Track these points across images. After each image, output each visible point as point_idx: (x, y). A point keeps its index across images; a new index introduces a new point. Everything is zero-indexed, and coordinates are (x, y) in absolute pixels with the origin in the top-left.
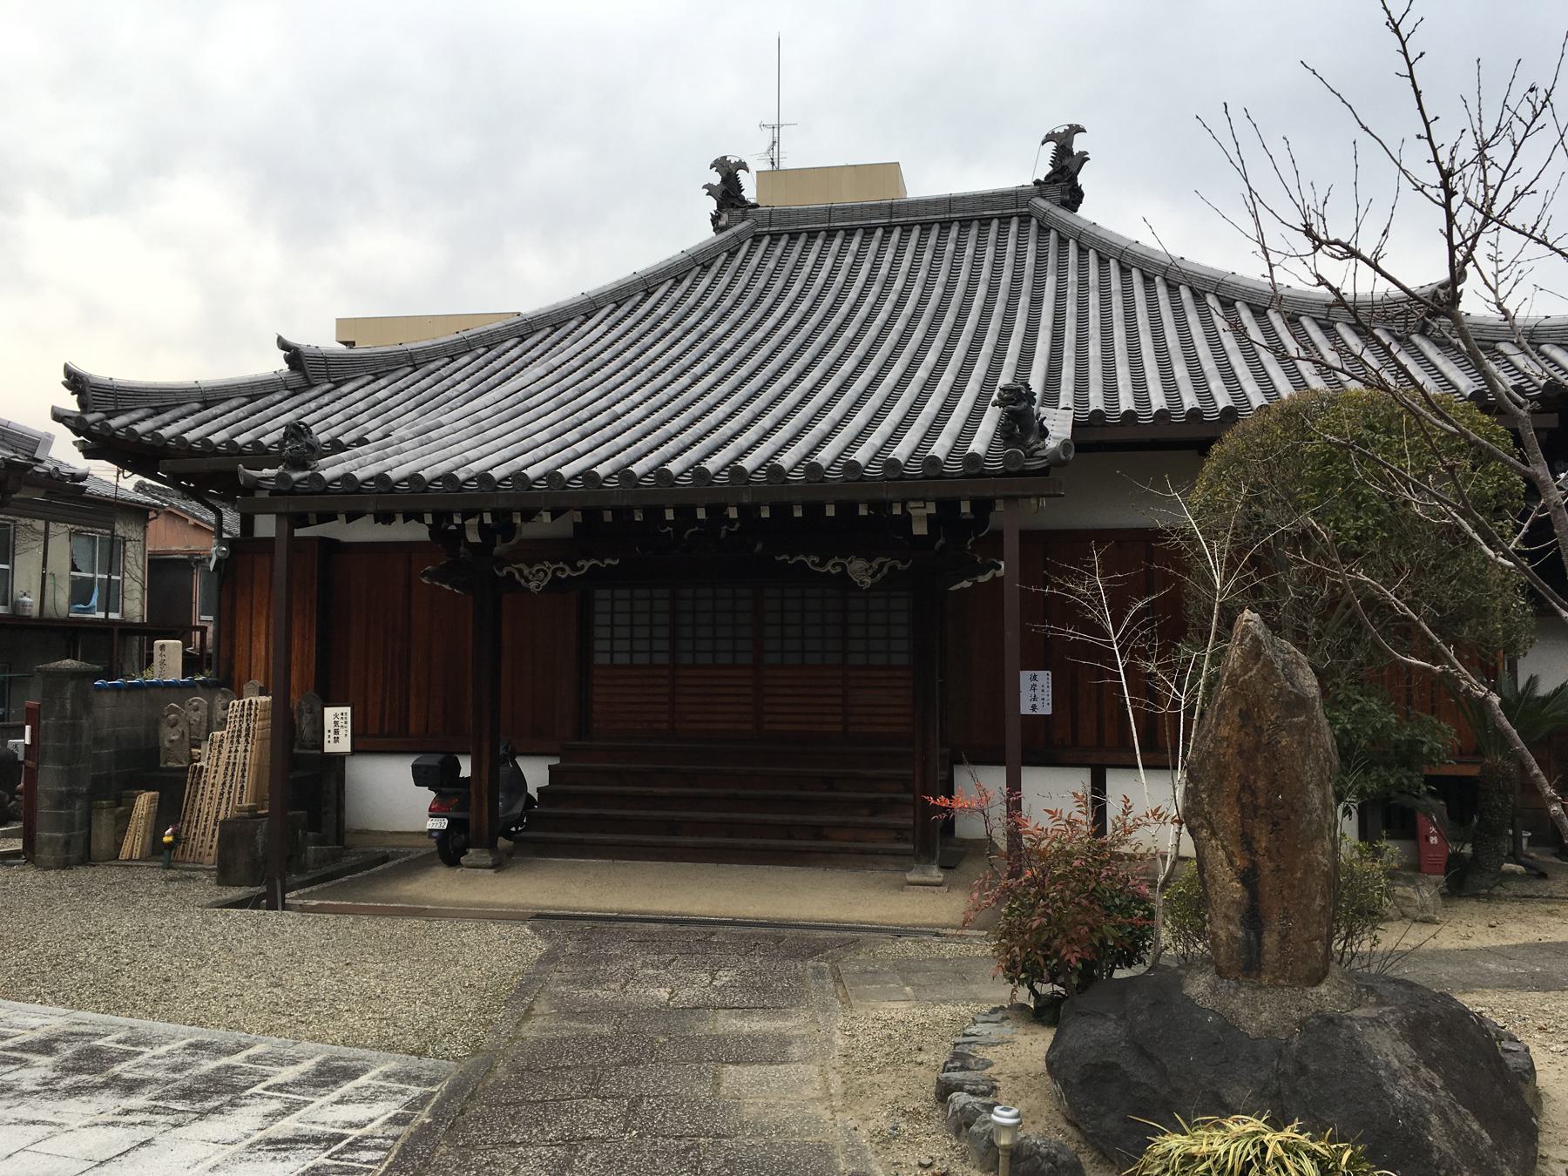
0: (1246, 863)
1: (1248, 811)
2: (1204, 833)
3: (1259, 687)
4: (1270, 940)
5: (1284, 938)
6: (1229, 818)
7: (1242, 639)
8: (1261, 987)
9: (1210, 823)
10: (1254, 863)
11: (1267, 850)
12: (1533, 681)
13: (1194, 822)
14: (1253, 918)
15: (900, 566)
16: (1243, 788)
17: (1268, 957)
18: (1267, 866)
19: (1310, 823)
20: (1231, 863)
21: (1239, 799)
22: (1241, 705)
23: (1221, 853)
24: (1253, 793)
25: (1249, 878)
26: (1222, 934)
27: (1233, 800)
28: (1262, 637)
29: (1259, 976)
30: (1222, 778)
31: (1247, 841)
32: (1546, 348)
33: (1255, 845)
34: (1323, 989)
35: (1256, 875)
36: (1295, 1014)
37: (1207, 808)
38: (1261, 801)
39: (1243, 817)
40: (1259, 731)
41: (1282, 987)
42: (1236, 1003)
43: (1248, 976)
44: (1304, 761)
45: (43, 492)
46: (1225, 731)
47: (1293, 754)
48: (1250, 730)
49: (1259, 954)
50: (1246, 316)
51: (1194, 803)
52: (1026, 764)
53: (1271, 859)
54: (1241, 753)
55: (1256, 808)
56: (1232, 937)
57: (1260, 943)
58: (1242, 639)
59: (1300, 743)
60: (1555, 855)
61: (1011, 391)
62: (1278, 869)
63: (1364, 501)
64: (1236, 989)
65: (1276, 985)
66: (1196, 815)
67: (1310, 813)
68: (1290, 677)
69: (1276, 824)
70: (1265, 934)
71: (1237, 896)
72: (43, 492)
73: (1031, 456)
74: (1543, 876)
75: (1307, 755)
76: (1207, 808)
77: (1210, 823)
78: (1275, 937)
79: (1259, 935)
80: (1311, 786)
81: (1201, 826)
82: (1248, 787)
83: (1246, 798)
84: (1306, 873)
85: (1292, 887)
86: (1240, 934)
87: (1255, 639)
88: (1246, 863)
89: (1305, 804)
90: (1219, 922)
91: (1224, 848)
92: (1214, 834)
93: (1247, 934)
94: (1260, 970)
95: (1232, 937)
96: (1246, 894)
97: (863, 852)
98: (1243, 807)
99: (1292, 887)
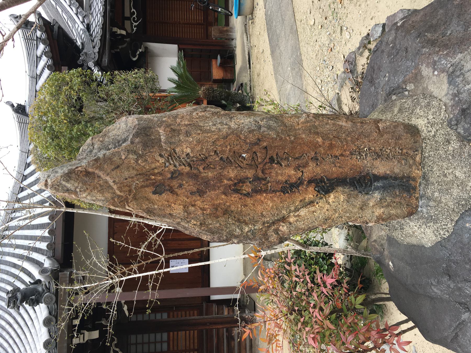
0: (311, 189)
1: (260, 186)
2: (284, 228)
3: (126, 174)
4: (381, 168)
5: (378, 155)
6: (267, 205)
7: (68, 190)
8: (424, 177)
9: (274, 223)
10: (310, 182)
11: (297, 168)
12: (171, 80)
13: (273, 238)
14: (361, 182)
15: (115, 342)
16: (237, 191)
17: (397, 170)
18: (312, 170)
19: (269, 128)
20: (311, 203)
21: (248, 195)
22: (149, 192)
23: (303, 212)
24: (242, 181)
25: (325, 186)
26: (379, 211)
27: (249, 201)
28: (66, 170)
29: (414, 179)
30: (226, 212)
31: (290, 188)
32: (38, 73)
33: (294, 180)
34: (421, 123)
35: (322, 180)
36: (455, 145)
37: (259, 226)
38: (250, 173)
39: (266, 191)
40: (175, 175)
41: (423, 158)
42: (448, 201)
43: (414, 189)
44: (210, 131)
45: (187, 261)
46: (178, 210)
47: (199, 142)
48: (175, 183)
49: (396, 178)
50: (26, 183)
51: (254, 239)
52: (209, 285)
53: (306, 165)
54: (201, 193)
55: (257, 178)
56: (380, 203)
57: (385, 177)
58: (68, 190)
59: (188, 134)
60: (233, 84)
61: (9, 302)
62: (315, 159)
63: (80, 131)
64: (429, 199)
65: (422, 164)
66: (265, 235)
67: (260, 127)
68: (118, 143)
69: (272, 160)
70: (375, 172)
71: (342, 197)
72: (187, 261)
73: (49, 289)
74: (242, 84)
75: (200, 128)
76: (259, 226)
77: (274, 223)
78: (377, 163)
79: (377, 178)
80: (232, 125)
81: (276, 231)
82: (236, 187)
83: (247, 188)
84: (317, 133)
85: (331, 147)
86: (377, 195)
87: (68, 176)
88: (311, 189)
89: (251, 131)
90: (367, 214)
91: (297, 210)
92: (283, 219)
93: (377, 189)
94: (409, 178)
95: (380, 203)
96: (340, 189)
97: (251, 346)
98: (257, 191)
99: (331, 147)
